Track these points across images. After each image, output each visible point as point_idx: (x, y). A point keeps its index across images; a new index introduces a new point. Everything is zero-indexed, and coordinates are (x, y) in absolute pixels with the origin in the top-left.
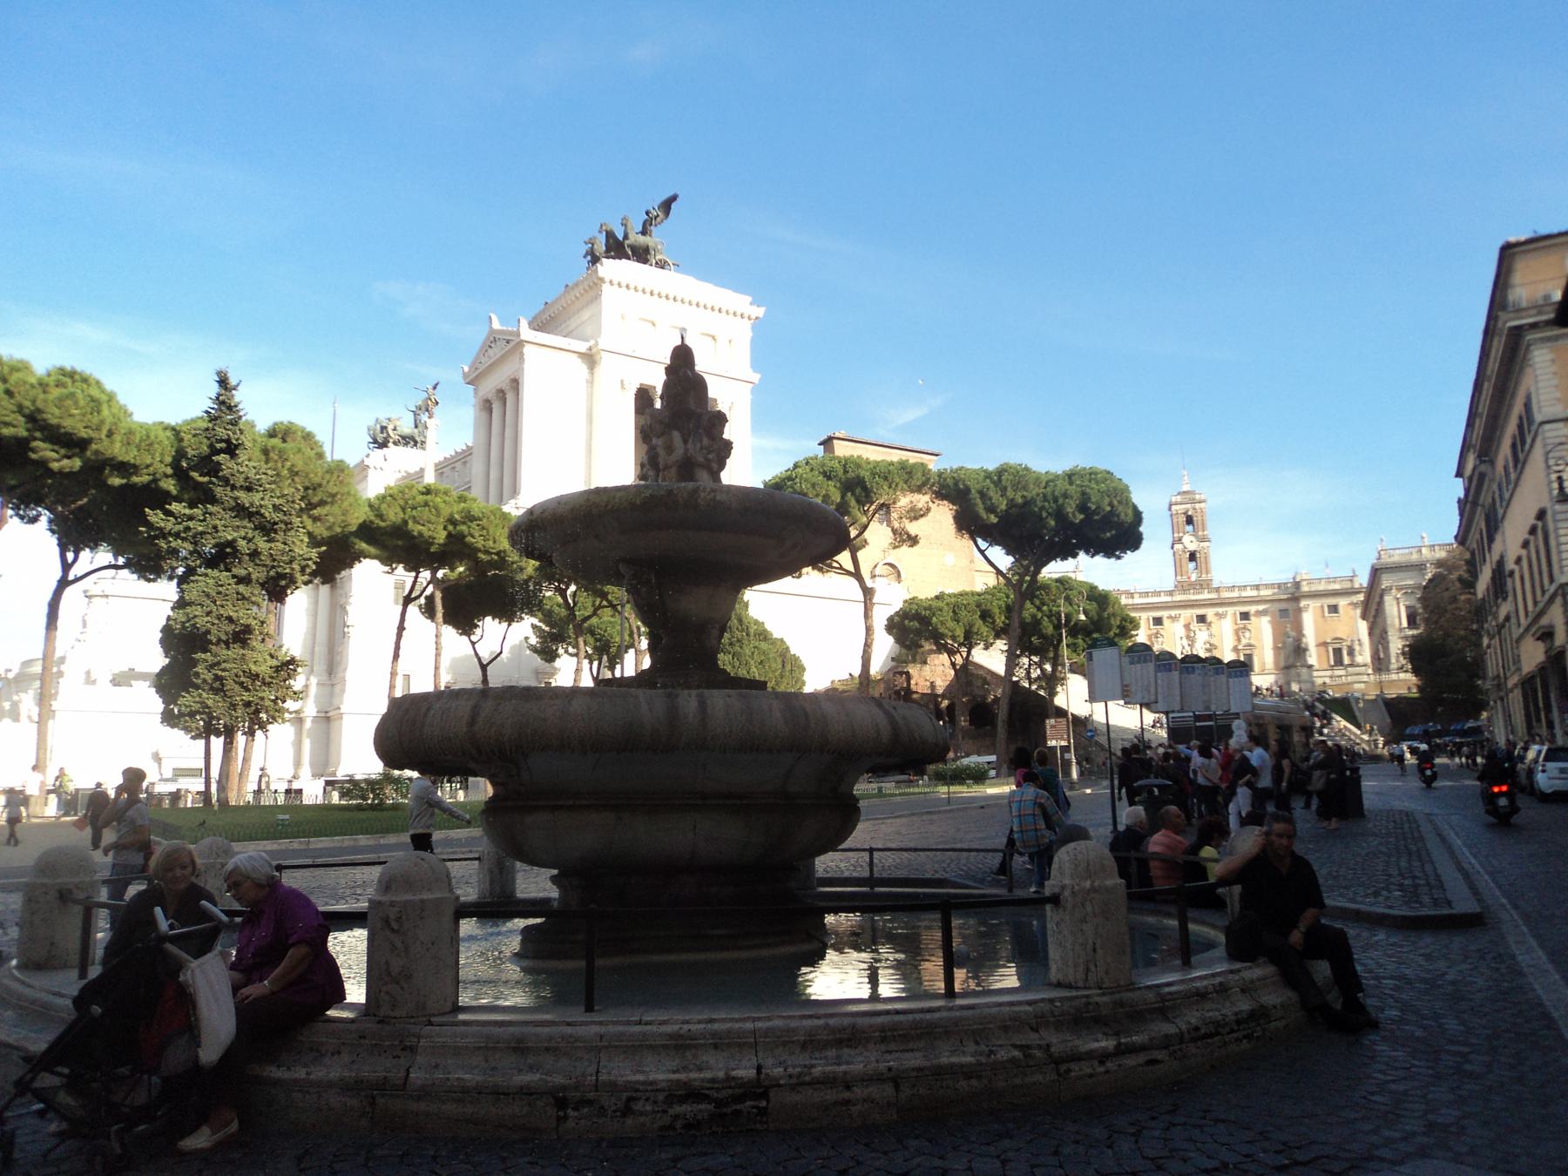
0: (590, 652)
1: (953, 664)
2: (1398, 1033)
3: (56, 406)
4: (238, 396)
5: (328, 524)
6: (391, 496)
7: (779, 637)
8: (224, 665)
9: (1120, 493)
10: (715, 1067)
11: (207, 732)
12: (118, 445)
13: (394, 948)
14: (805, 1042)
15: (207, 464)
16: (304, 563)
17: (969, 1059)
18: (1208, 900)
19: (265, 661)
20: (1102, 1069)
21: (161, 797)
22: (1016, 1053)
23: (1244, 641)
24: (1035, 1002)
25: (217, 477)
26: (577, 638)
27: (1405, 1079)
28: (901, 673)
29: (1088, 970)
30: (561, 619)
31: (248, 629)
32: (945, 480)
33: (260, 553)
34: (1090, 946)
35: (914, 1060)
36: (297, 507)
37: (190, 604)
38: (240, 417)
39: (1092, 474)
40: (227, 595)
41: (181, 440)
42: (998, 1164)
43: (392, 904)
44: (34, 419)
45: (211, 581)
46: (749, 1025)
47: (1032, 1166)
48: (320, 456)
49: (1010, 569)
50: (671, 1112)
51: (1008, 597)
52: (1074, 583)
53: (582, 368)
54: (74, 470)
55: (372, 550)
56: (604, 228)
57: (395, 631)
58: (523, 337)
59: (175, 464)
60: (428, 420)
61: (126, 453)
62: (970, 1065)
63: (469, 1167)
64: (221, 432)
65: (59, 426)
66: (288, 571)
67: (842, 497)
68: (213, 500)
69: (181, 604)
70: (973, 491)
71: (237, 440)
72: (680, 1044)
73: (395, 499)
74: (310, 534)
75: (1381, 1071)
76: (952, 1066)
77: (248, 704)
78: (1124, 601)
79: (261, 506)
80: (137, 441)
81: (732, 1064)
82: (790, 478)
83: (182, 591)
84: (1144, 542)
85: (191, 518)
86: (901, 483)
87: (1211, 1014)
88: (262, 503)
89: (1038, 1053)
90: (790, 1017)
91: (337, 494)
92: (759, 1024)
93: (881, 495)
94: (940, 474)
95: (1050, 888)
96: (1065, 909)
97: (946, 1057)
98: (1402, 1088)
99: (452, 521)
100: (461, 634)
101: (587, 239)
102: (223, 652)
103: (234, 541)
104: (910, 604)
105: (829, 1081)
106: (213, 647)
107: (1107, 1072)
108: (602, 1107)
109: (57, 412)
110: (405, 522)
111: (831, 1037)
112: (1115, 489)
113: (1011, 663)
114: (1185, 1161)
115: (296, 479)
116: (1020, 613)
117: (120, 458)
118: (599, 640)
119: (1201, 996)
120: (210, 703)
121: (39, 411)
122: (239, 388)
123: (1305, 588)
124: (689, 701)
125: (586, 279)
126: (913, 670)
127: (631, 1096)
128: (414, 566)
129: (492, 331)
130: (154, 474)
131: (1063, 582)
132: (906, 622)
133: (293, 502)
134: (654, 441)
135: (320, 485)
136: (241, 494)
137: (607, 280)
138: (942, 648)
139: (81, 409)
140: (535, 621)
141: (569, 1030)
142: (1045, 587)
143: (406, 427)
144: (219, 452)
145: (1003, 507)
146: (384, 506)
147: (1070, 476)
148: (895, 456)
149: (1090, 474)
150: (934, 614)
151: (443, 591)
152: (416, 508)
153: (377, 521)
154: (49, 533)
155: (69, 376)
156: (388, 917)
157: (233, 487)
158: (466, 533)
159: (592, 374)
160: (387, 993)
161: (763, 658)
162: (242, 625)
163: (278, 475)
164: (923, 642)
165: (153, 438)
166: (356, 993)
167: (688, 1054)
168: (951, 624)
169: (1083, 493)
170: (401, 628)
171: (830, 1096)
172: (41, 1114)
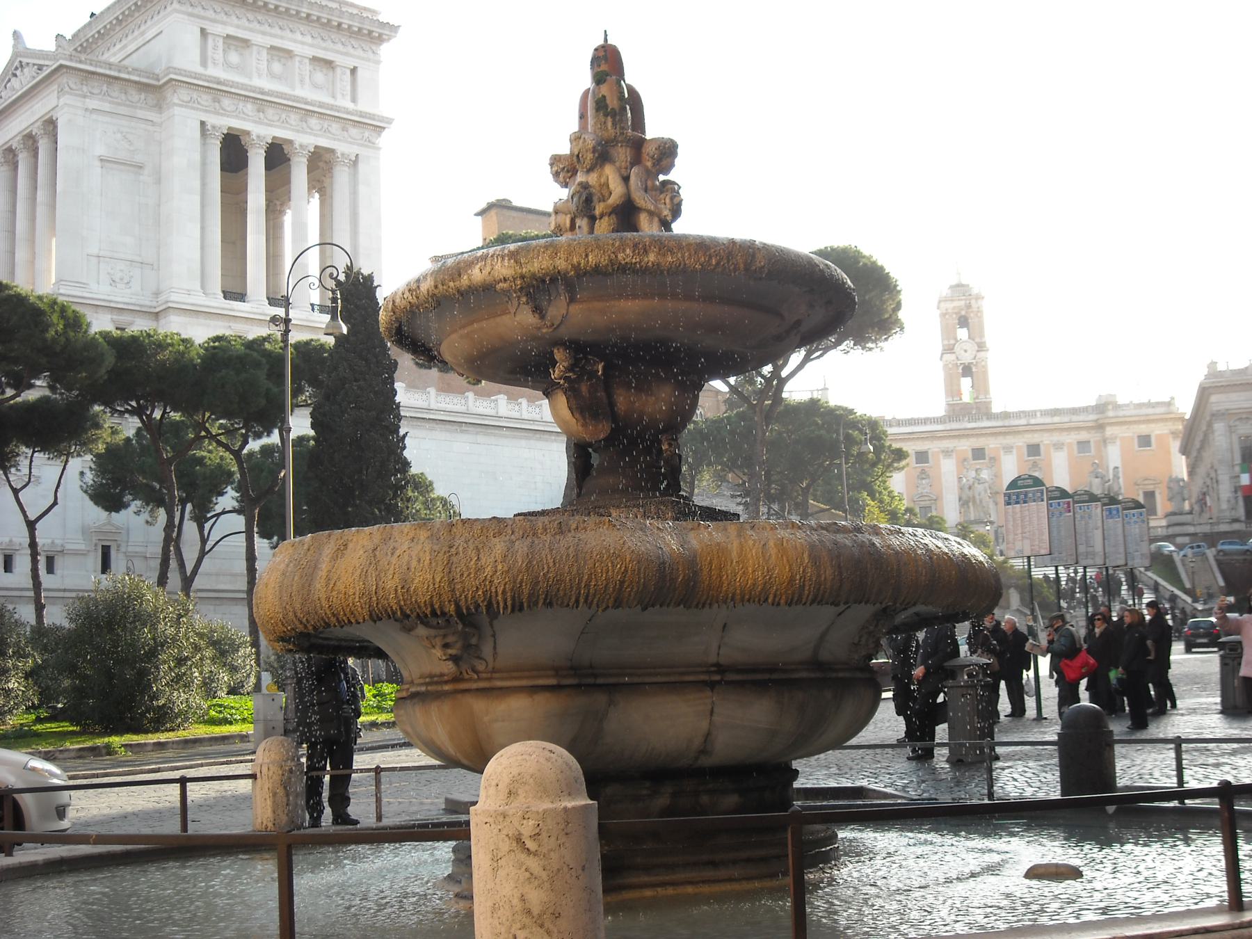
156: (520, 834)
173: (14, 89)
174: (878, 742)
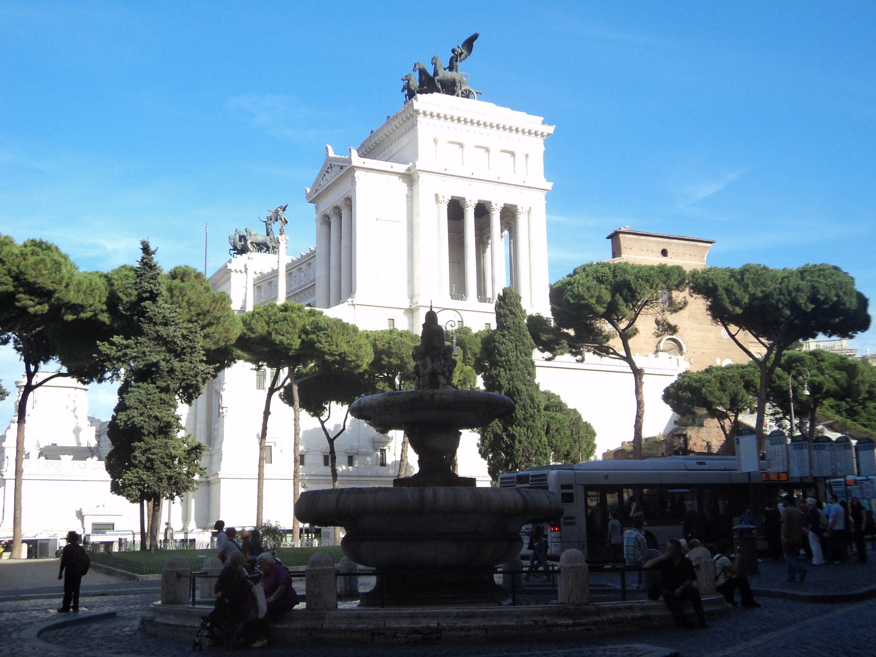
3: (33, 269)
5: (214, 339)
6: (258, 313)
7: (572, 408)
8: (153, 451)
9: (844, 283)
10: (424, 623)
15: (136, 307)
16: (204, 376)
17: (513, 624)
20: (566, 630)
21: (95, 545)
22: (532, 623)
25: (144, 317)
28: (679, 436)
29: (569, 597)
32: (697, 280)
33: (175, 370)
37: (129, 408)
38: (158, 274)
39: (821, 271)
40: (154, 401)
41: (112, 285)
44: (18, 278)
45: (143, 391)
52: (826, 355)
53: (403, 187)
54: (44, 312)
55: (245, 355)
56: (417, 67)
57: (262, 415)
58: (354, 163)
60: (280, 237)
61: (78, 298)
65: (35, 283)
66: (194, 382)
68: (141, 333)
69: (121, 407)
70: (720, 288)
71: (157, 290)
72: (412, 616)
73: (261, 316)
79: (174, 336)
80: (84, 289)
82: (569, 283)
85: (127, 347)
86: (661, 285)
88: (175, 334)
91: (221, 317)
93: (644, 294)
99: (304, 331)
100: (313, 416)
102: (153, 442)
103: (158, 362)
104: (684, 377)
105: (462, 629)
106: (145, 438)
109: (33, 273)
110: (270, 334)
112: (840, 282)
115: (192, 308)
117: (73, 302)
120: (145, 477)
121: (21, 273)
122: (156, 252)
125: (404, 111)
126: (691, 432)
128: (276, 364)
129: (329, 159)
130: (95, 311)
132: (680, 392)
133: (196, 332)
135: (208, 312)
136: (160, 328)
137: (421, 111)
139: (49, 269)
143: (261, 237)
144: (145, 299)
145: (746, 300)
146: (253, 321)
147: (802, 273)
149: (820, 270)
150: (703, 386)
152: (278, 322)
154: (15, 351)
155: (39, 246)
158: (316, 340)
159: (412, 190)
161: (559, 426)
162: (165, 422)
165: (94, 285)
168: (718, 393)
169: (813, 287)
170: (267, 413)
171: (463, 633)
173: (327, 180)
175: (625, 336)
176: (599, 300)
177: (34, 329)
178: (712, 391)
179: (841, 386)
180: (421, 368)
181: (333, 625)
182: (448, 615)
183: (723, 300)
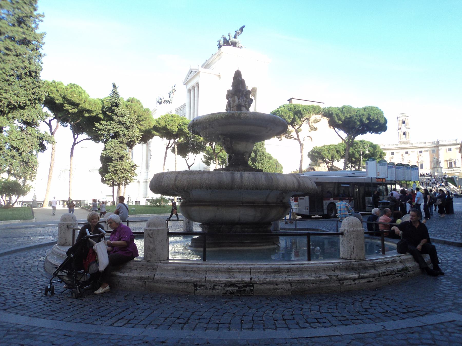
0: (220, 163)
1: (328, 166)
2: (450, 277)
4: (118, 90)
8: (117, 166)
9: (380, 114)
10: (239, 278)
11: (113, 184)
12: (87, 105)
13: (151, 242)
14: (265, 272)
16: (137, 137)
17: (313, 278)
18: (393, 235)
19: (128, 165)
20: (353, 283)
22: (328, 277)
23: (420, 160)
24: (334, 263)
25: (113, 113)
26: (216, 158)
27: (450, 290)
28: (312, 169)
29: (351, 254)
30: (211, 153)
31: (123, 156)
34: (352, 247)
35: (297, 278)
36: (135, 121)
37: (107, 149)
38: (119, 96)
39: (372, 108)
41: (104, 103)
42: (318, 307)
43: (150, 230)
45: (113, 143)
46: (249, 266)
47: (328, 309)
48: (142, 107)
49: (346, 138)
50: (226, 289)
51: (345, 146)
55: (157, 133)
59: (102, 110)
62: (313, 280)
63: (169, 301)
64: (114, 101)
65: (71, 100)
67: (294, 116)
68: (112, 119)
69: (105, 149)
70: (334, 114)
72: (229, 271)
74: (140, 130)
75: (442, 287)
76: (308, 280)
77: (123, 177)
78: (382, 147)
81: (243, 277)
82: (278, 111)
83: (105, 146)
84: (388, 129)
85: (107, 125)
87: (389, 268)
89: (334, 277)
90: (260, 264)
92: (252, 266)
94: (324, 109)
95: (340, 231)
96: (345, 236)
97: (306, 277)
98: (448, 292)
101: (218, 40)
102: (116, 162)
103: (119, 131)
105: (271, 283)
107: (355, 284)
108: (207, 287)
109: (70, 96)
110: (166, 126)
111: (272, 271)
112: (379, 113)
113: (346, 166)
114: (375, 309)
116: (348, 151)
117: (88, 109)
118: (223, 159)
119: (387, 263)
120: (113, 177)
121: (65, 95)
123: (441, 143)
124: (237, 175)
127: (215, 285)
128: (169, 138)
131: (362, 141)
133: (134, 120)
134: (230, 99)
135: (142, 115)
136: (120, 118)
138: (324, 161)
140: (204, 154)
141: (198, 266)
142: (356, 143)
143: (167, 98)
144: (113, 106)
145: (344, 119)
146: (160, 121)
147: (365, 109)
148: (310, 104)
149: (371, 108)
151: (177, 145)
153: (158, 125)
157: (118, 116)
158: (183, 128)
160: (149, 254)
163: (130, 112)
164: (319, 160)
166: (141, 253)
167: (231, 273)
168: (327, 154)
169: (369, 114)
170: (166, 156)
171: (271, 287)
172: (61, 282)
174: (142, 222)
175: (297, 132)
176: (289, 117)
177: (76, 121)
178: (325, 154)
179: (371, 153)
180: (231, 102)
181: (163, 276)
182: (259, 271)
183: (335, 118)
